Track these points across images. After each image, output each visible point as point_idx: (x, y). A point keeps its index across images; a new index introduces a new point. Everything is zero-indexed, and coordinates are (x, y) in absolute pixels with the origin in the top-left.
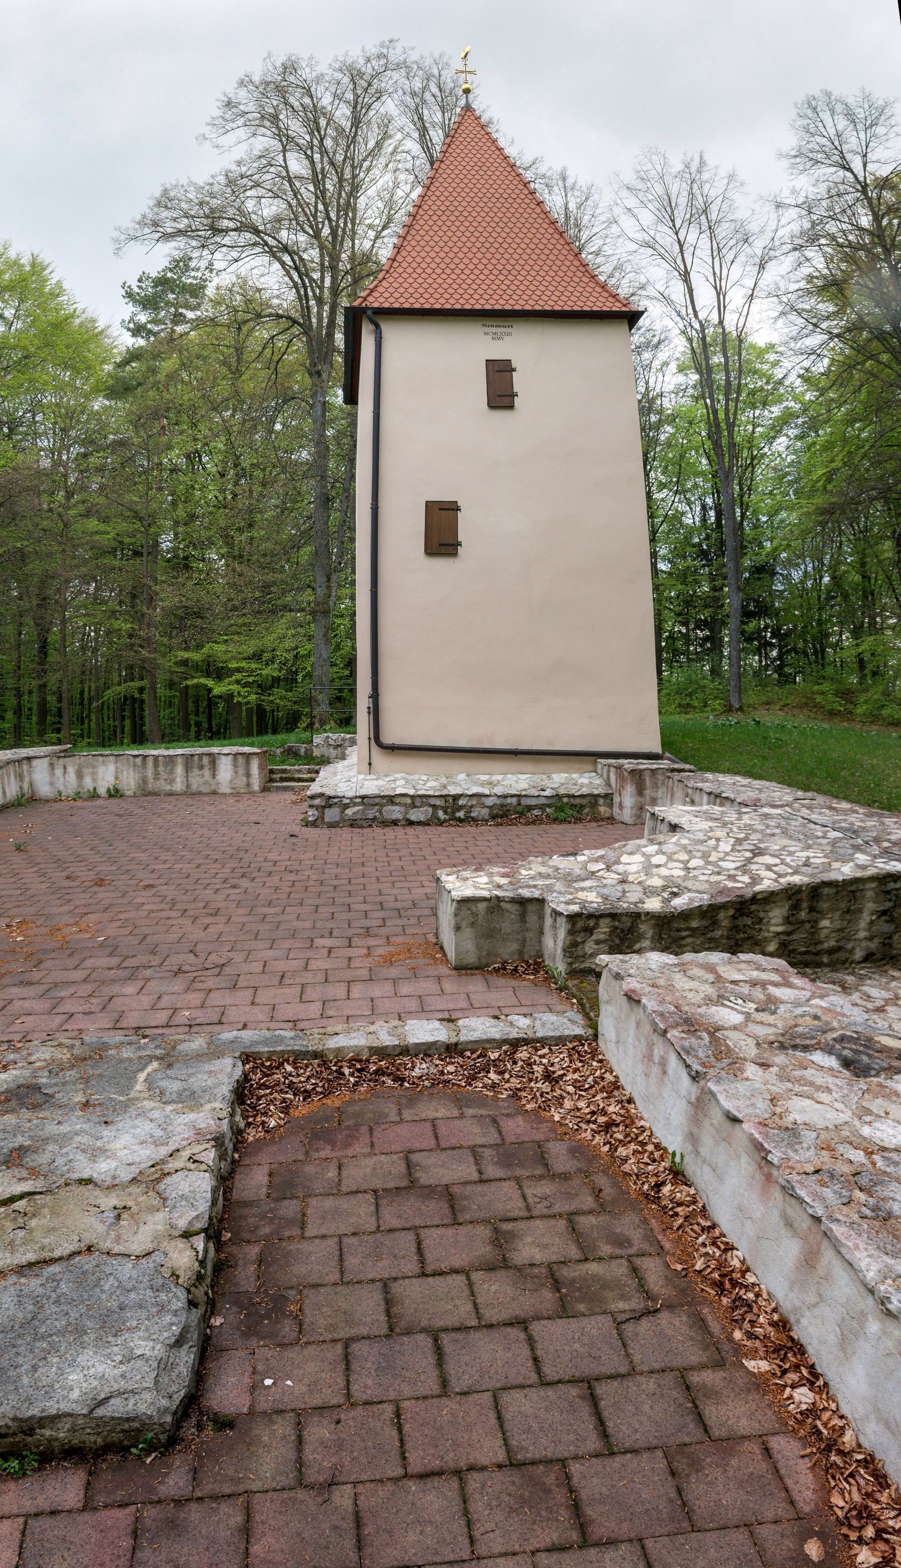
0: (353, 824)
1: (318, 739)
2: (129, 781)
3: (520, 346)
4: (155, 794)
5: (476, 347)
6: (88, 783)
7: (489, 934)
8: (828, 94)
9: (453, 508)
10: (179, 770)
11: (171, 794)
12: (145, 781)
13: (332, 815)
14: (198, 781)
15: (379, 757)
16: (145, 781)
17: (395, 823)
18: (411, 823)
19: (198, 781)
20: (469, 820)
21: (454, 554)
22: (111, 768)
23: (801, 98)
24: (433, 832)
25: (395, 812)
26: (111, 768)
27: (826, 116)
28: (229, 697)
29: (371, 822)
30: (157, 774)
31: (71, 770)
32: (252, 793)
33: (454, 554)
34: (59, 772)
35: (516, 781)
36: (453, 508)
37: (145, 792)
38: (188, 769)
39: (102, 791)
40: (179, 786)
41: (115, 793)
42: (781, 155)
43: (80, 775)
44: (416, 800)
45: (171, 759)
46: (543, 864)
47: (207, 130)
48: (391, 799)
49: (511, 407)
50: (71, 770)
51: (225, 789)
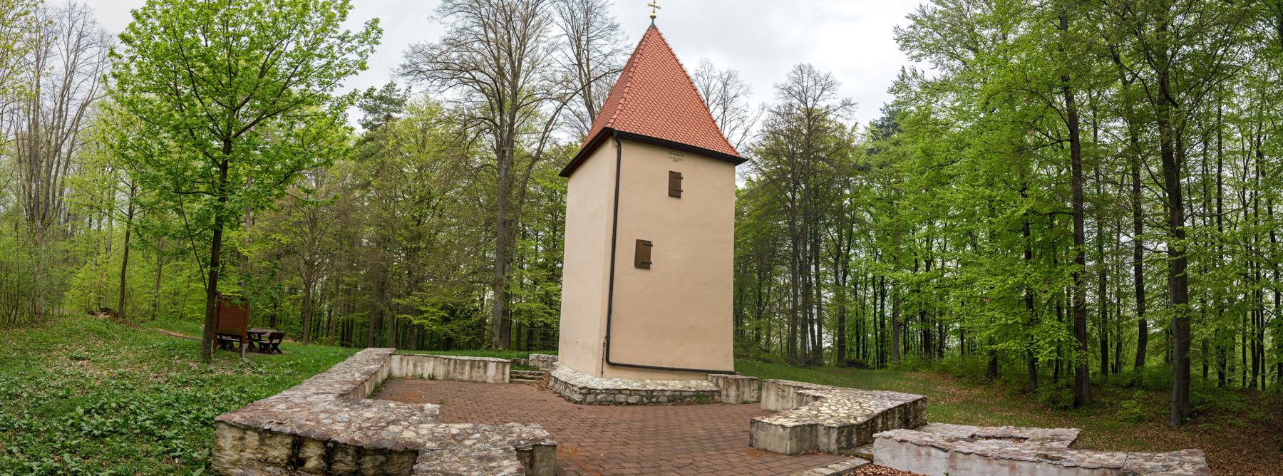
0: (601, 403)
1: (533, 356)
2: (440, 372)
3: (689, 169)
4: (452, 380)
5: (664, 164)
6: (419, 371)
7: (801, 440)
8: (810, 67)
9: (649, 244)
10: (467, 368)
11: (462, 381)
12: (448, 372)
13: (590, 398)
14: (477, 375)
15: (607, 370)
16: (448, 372)
17: (621, 403)
18: (629, 404)
19: (477, 375)
20: (658, 403)
21: (648, 268)
22: (432, 363)
23: (797, 64)
24: (638, 409)
25: (621, 398)
26: (432, 363)
27: (805, 76)
28: (420, 326)
29: (609, 403)
30: (455, 369)
31: (411, 363)
32: (504, 383)
33: (648, 268)
34: (405, 363)
35: (675, 384)
36: (649, 244)
37: (448, 378)
38: (472, 368)
39: (426, 376)
40: (466, 377)
41: (432, 378)
42: (776, 86)
43: (415, 366)
44: (633, 392)
45: (463, 362)
46: (800, 416)
47: (434, 14)
48: (620, 391)
49: (679, 197)
50: (411, 363)
51: (490, 380)
